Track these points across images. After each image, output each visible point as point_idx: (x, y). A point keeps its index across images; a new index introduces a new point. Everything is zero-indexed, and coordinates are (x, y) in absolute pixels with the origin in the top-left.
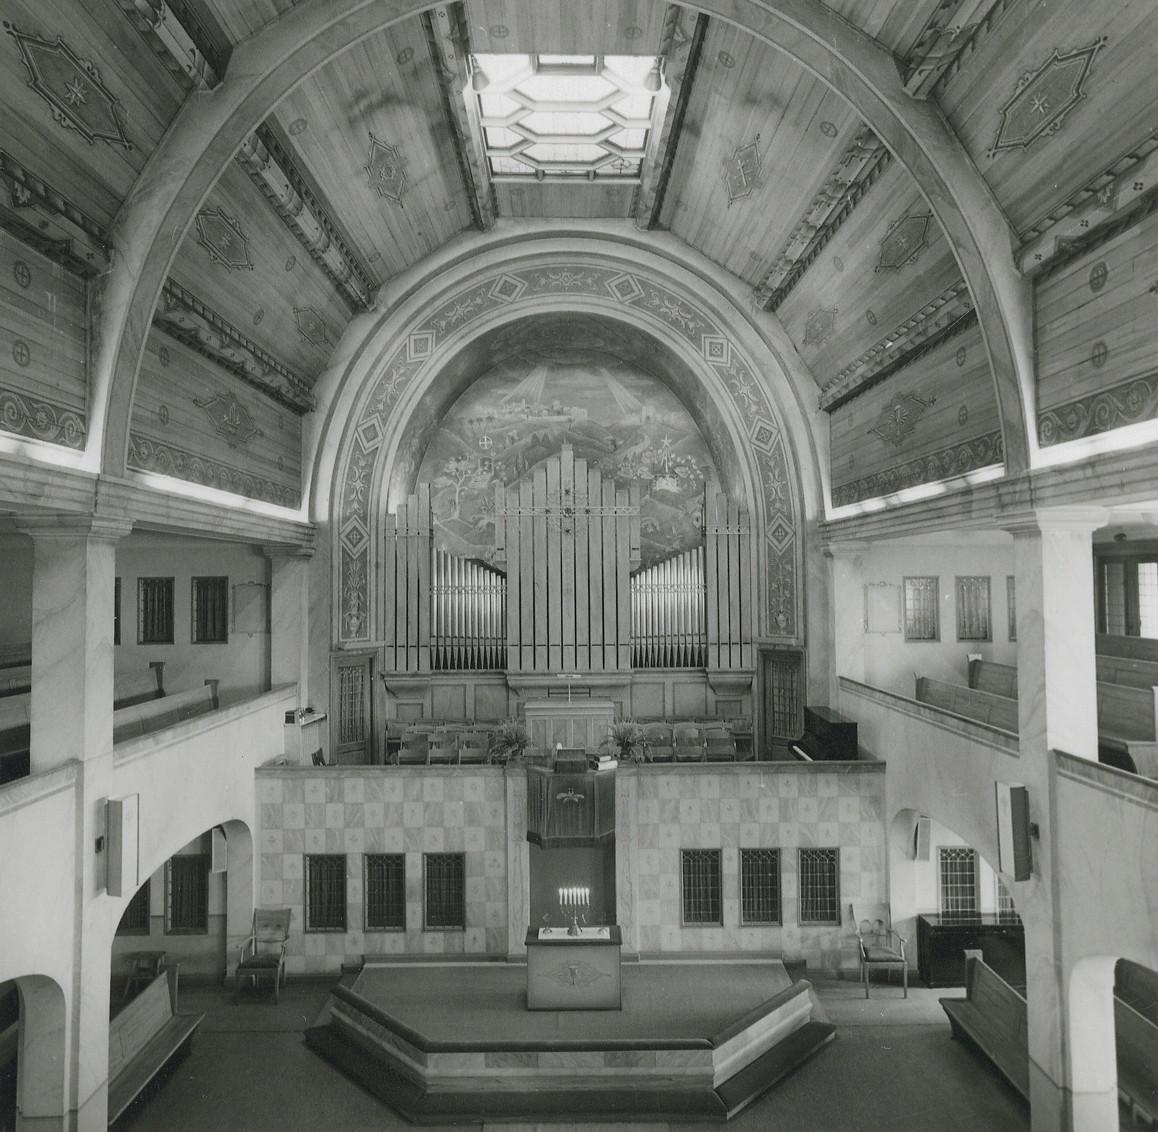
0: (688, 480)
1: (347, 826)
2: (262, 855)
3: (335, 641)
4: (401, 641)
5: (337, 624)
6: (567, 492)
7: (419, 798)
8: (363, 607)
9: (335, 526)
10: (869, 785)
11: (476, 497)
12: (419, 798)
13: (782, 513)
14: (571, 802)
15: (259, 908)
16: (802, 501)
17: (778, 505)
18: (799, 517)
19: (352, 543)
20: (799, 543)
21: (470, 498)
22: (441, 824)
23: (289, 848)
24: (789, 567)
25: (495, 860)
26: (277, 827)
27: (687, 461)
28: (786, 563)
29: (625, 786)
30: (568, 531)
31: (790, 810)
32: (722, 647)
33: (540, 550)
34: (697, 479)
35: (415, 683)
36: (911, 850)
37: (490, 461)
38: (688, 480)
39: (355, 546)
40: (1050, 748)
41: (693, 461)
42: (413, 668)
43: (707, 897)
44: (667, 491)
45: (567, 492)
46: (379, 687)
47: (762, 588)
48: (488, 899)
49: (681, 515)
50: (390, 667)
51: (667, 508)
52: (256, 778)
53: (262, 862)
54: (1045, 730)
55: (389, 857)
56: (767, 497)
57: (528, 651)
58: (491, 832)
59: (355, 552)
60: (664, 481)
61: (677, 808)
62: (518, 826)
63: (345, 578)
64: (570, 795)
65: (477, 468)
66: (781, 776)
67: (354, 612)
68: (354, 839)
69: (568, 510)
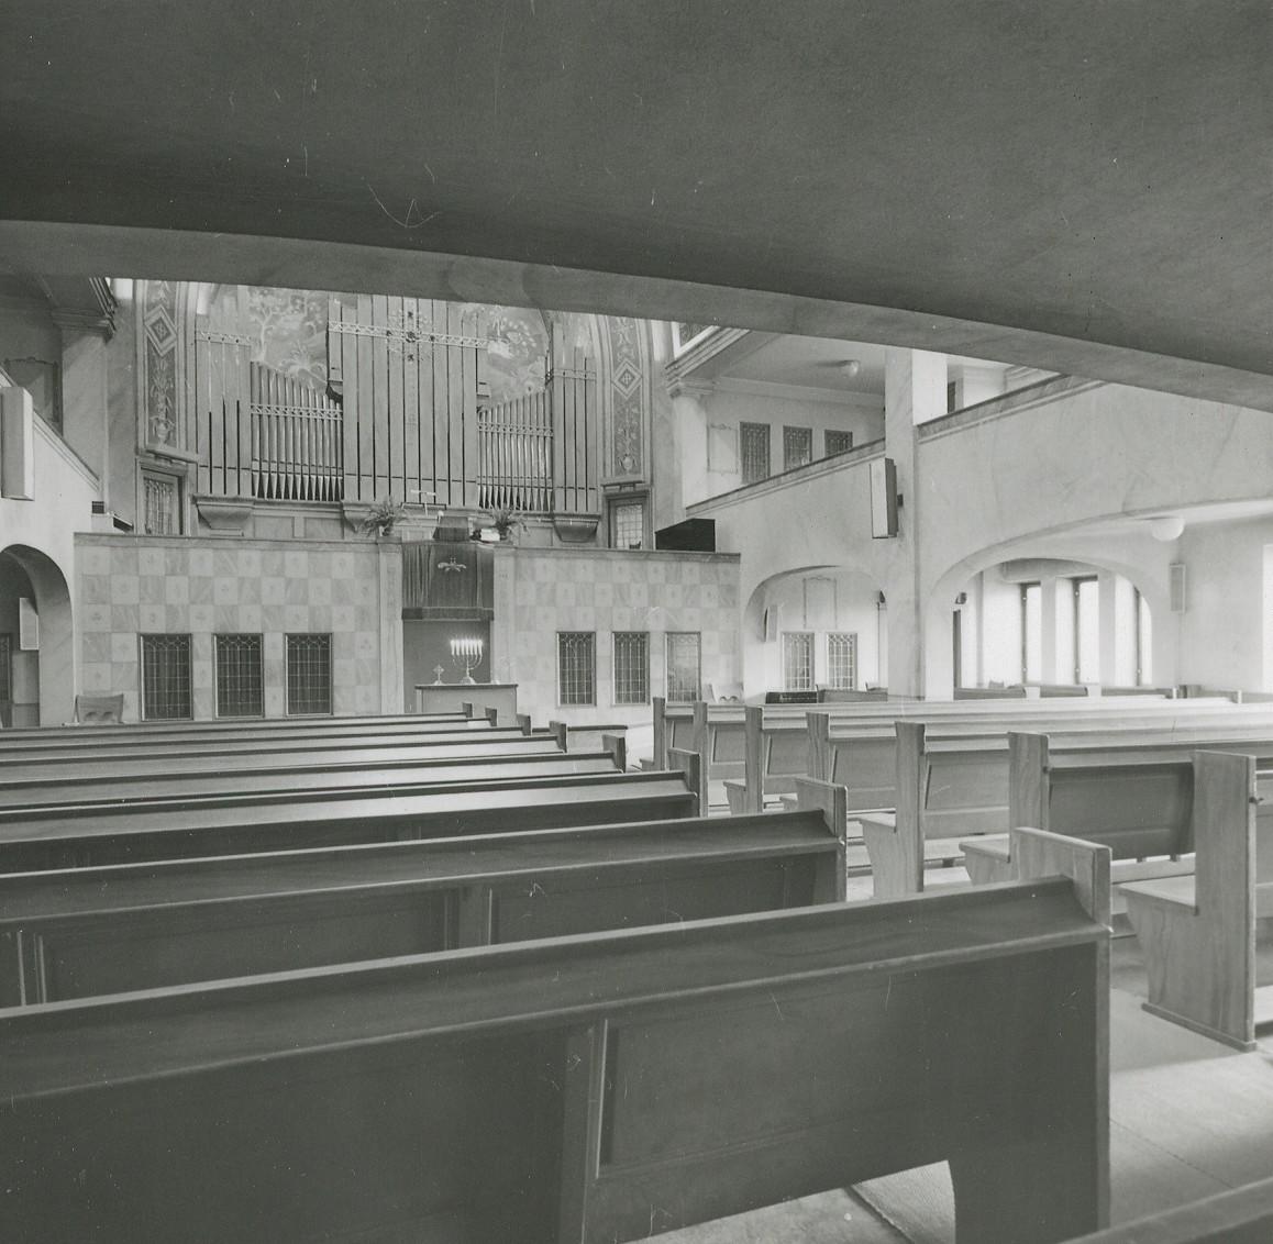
0: (519, 346)
1: (193, 603)
2: (84, 634)
3: (141, 445)
4: (218, 460)
5: (143, 425)
6: (410, 314)
7: (280, 573)
8: (171, 414)
9: (139, 309)
10: (726, 573)
11: (285, 340)
12: (280, 573)
13: (629, 357)
14: (453, 571)
15: (81, 694)
16: (650, 344)
17: (625, 350)
18: (646, 360)
19: (158, 337)
20: (647, 385)
21: (277, 338)
22: (305, 602)
23: (119, 628)
24: (635, 410)
25: (366, 642)
26: (104, 603)
27: (520, 327)
28: (633, 407)
29: (503, 566)
30: (411, 357)
31: (654, 596)
32: (569, 491)
33: (381, 375)
34: (529, 346)
35: (236, 510)
36: (763, 636)
37: (303, 299)
38: (519, 346)
39: (161, 341)
40: (915, 424)
41: (526, 328)
42: (232, 493)
43: (579, 672)
44: (500, 356)
45: (410, 314)
46: (190, 511)
47: (608, 434)
48: (359, 682)
49: (513, 382)
50: (204, 491)
51: (499, 373)
52: (75, 545)
53: (85, 642)
54: (911, 410)
55: (244, 637)
56: (614, 343)
57: (367, 481)
58: (363, 613)
59: (163, 348)
60: (496, 345)
61: (554, 591)
62: (391, 604)
63: (152, 375)
64: (452, 564)
65: (286, 306)
66: (650, 563)
67: (162, 417)
68: (201, 617)
69: (411, 334)
